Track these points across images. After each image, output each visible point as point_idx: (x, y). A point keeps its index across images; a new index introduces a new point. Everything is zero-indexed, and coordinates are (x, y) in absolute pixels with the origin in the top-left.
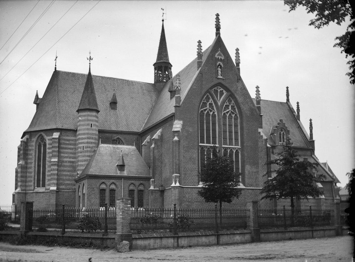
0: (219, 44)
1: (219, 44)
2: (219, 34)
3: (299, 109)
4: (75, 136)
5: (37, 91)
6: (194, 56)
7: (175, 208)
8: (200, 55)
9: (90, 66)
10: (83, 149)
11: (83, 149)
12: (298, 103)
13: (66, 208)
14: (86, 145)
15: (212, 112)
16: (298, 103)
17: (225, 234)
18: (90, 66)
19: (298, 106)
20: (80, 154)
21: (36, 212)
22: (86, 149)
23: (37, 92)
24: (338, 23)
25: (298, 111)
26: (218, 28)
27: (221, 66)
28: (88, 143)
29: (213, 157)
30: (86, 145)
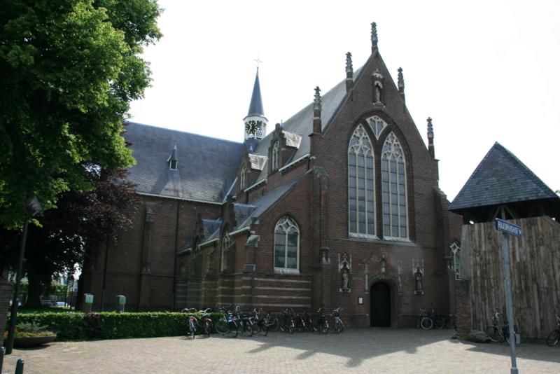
0: (376, 60)
1: (376, 60)
2: (377, 48)
3: (432, 133)
6: (343, 76)
8: (350, 74)
12: (429, 120)
13: (147, 270)
15: (456, 250)
16: (429, 120)
19: (430, 125)
24: (373, 94)
25: (431, 136)
27: (379, 87)
29: (8, 275)
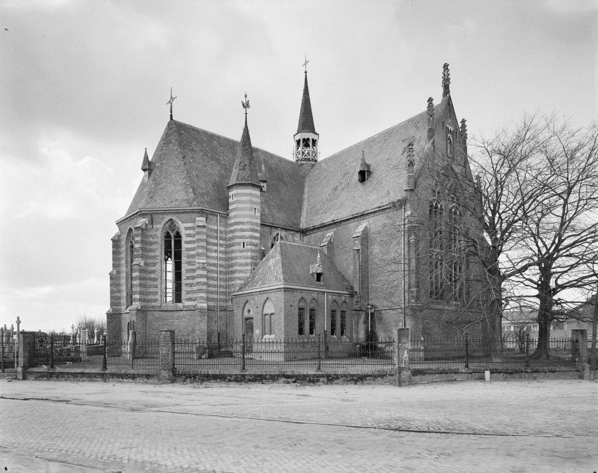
4: (227, 225)
5: (146, 149)
7: (244, 339)
9: (246, 117)
10: (244, 247)
11: (244, 247)
14: (248, 240)
17: (463, 373)
18: (246, 117)
20: (238, 254)
21: (563, 342)
22: (249, 247)
23: (146, 152)
26: (171, 112)
28: (251, 237)
30: (248, 240)
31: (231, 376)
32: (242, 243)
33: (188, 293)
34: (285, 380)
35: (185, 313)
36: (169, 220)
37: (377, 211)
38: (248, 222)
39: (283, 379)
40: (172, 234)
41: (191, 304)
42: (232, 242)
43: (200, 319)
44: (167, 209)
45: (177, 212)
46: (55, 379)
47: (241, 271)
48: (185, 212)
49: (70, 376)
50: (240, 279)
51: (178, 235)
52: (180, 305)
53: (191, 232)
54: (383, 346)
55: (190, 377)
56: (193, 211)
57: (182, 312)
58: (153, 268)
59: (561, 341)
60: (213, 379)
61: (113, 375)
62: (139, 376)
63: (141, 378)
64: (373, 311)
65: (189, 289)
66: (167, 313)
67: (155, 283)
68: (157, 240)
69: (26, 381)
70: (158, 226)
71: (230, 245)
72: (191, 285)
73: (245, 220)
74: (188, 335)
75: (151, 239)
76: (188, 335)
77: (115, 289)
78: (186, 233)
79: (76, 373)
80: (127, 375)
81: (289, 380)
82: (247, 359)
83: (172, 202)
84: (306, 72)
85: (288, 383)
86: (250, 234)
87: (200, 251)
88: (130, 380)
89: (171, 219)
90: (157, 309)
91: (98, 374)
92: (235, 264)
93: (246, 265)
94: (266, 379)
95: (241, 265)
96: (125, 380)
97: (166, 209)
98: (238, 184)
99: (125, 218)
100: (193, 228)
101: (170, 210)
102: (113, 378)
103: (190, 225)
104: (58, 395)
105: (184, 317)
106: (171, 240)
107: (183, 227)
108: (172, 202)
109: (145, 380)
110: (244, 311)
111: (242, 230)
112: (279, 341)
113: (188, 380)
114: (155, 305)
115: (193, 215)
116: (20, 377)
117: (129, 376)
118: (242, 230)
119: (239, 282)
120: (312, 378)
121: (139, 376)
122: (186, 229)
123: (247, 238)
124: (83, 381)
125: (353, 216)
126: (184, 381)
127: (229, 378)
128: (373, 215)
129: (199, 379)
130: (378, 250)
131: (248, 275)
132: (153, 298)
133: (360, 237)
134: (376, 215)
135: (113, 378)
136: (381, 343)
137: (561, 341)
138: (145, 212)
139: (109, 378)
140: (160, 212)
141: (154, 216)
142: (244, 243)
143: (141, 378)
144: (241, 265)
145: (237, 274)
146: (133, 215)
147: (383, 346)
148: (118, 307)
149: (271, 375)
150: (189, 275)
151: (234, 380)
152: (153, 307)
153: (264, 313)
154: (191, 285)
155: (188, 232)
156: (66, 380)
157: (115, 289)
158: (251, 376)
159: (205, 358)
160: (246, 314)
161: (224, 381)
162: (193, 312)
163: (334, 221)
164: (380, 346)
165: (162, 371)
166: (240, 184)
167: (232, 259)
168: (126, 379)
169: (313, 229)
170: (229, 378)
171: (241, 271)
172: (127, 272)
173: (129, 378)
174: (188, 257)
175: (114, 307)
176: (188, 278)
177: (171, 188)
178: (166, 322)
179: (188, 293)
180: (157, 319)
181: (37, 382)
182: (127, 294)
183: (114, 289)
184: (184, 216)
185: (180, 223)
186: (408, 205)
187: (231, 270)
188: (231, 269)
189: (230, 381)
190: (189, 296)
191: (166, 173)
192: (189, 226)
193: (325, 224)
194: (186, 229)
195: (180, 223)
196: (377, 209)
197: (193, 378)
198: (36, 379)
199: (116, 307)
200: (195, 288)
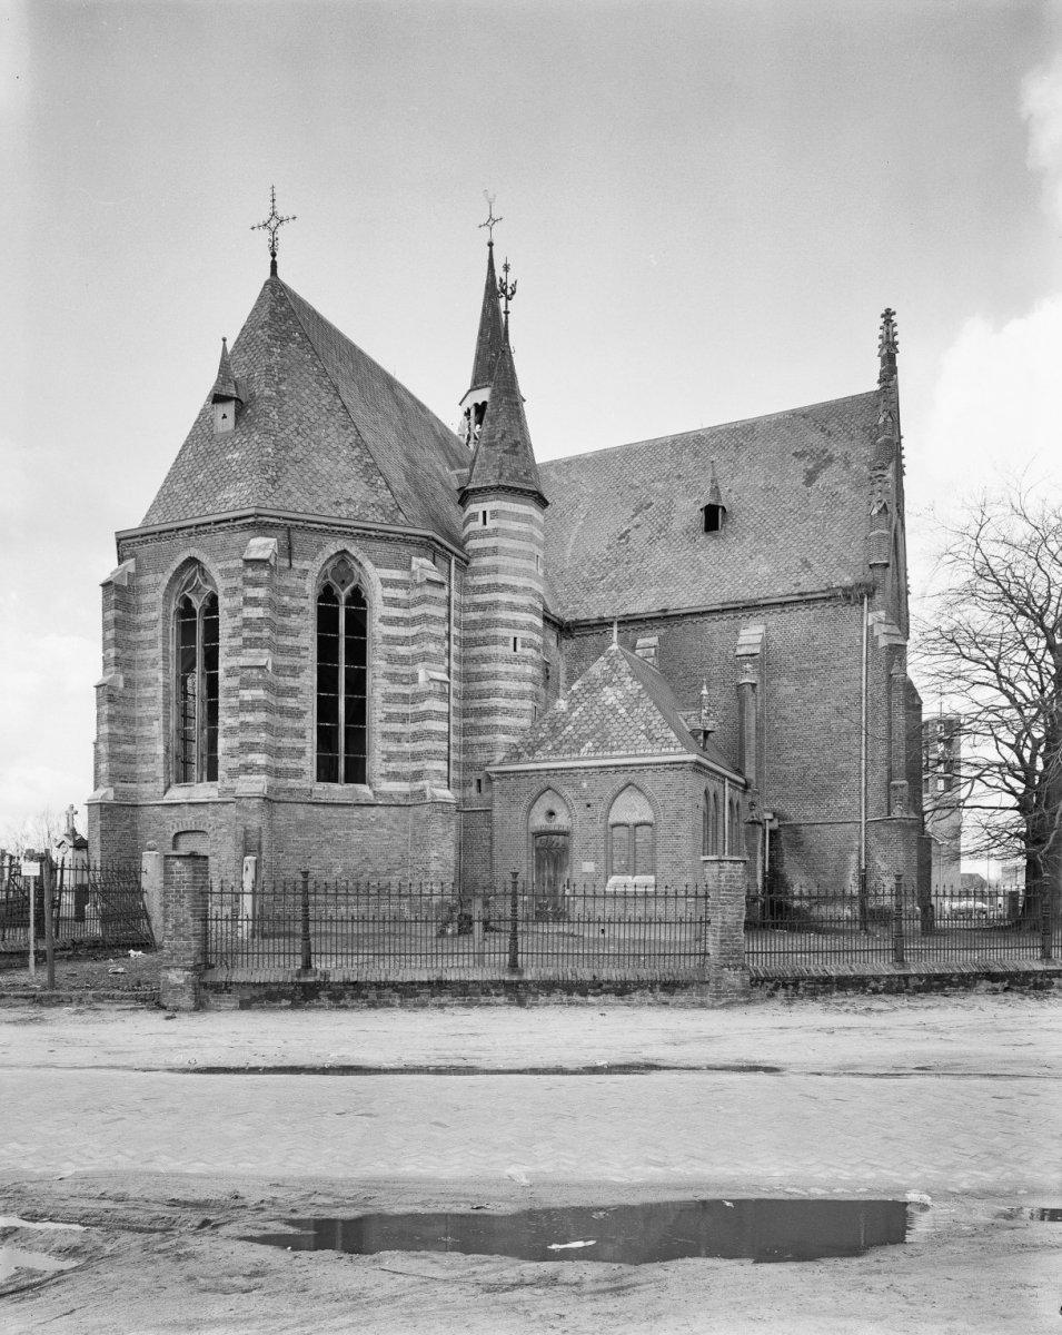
10: (515, 650)
11: (515, 650)
20: (502, 668)
26: (274, 255)
31: (877, 979)
32: (512, 640)
33: (390, 757)
34: (990, 985)
35: (382, 812)
36: (338, 553)
37: (793, 602)
38: (525, 588)
39: (985, 984)
40: (197, 604)
41: (398, 789)
42: (482, 634)
43: (440, 831)
44: (338, 522)
45: (364, 535)
46: (325, 1001)
47: (507, 712)
48: (385, 538)
49: (387, 991)
50: (506, 730)
51: (357, 598)
52: (364, 789)
53: (400, 594)
54: (806, 904)
55: (785, 986)
56: (406, 540)
57: (373, 810)
58: (291, 682)
59: (948, 893)
60: (839, 990)
61: (549, 987)
62: (640, 985)
63: (647, 991)
64: (775, 825)
65: (393, 748)
66: (331, 809)
67: (298, 725)
68: (303, 603)
69: (208, 1015)
70: (306, 564)
71: (475, 640)
72: (397, 737)
73: (520, 582)
74: (390, 872)
75: (286, 599)
76: (390, 872)
77: (121, 732)
78: (386, 595)
79: (413, 983)
80: (600, 985)
81: (997, 985)
82: (315, 934)
83: (338, 504)
84: (491, 245)
85: (995, 992)
86: (529, 620)
87: (432, 647)
88: (611, 998)
89: (345, 551)
90: (303, 798)
91: (496, 984)
92: (494, 693)
93: (522, 696)
94: (951, 984)
95: (508, 695)
96: (591, 999)
97: (334, 521)
98: (504, 488)
99: (137, 533)
100: (403, 584)
101: (344, 526)
102: (548, 995)
103: (397, 574)
104: (464, 1053)
105: (379, 822)
106: (337, 609)
107: (376, 579)
108: (338, 504)
109: (663, 997)
110: (536, 808)
111: (512, 607)
112: (671, 892)
113: (781, 993)
114: (298, 786)
115: (405, 550)
116: (186, 1000)
117: (605, 986)
118: (512, 607)
119: (502, 738)
120: (1039, 980)
121: (640, 985)
122: (386, 583)
123: (522, 628)
124: (441, 1006)
125: (724, 607)
126: (771, 996)
127: (873, 984)
128: (779, 610)
129: (806, 989)
130: (791, 690)
131: (525, 722)
132: (291, 766)
133: (757, 657)
134: (787, 609)
135: (548, 995)
136: (800, 898)
137: (948, 893)
138: (272, 520)
139: (535, 995)
140: (315, 525)
141: (297, 536)
142: (515, 639)
143: (647, 991)
144: (508, 695)
145: (499, 717)
146: (217, 523)
147: (806, 904)
148: (129, 785)
149: (962, 975)
150: (393, 709)
151: (883, 990)
152: (291, 790)
153: (611, 820)
154: (397, 737)
155: (391, 593)
156: (372, 1005)
157: (121, 732)
158: (920, 977)
159: (453, 935)
160: (539, 821)
161: (863, 992)
162: (402, 810)
163: (665, 610)
164: (796, 903)
165: (726, 969)
166: (510, 488)
167: (479, 677)
168: (595, 995)
169: (596, 625)
170: (873, 984)
171: (507, 712)
172: (166, 686)
173: (607, 992)
174: (391, 659)
175: (120, 785)
176: (389, 718)
177: (323, 465)
178: (328, 834)
179: (390, 757)
180: (302, 827)
181: (245, 1015)
182: (167, 749)
183: (118, 732)
184: (380, 548)
185: (368, 565)
186: (877, 597)
187: (477, 706)
188: (477, 704)
189: (875, 991)
190: (392, 767)
191: (300, 422)
192: (394, 577)
193: (636, 617)
194: (386, 583)
195: (368, 565)
196: (797, 598)
197: (791, 987)
198: (245, 1005)
199: (124, 785)
200: (408, 747)
